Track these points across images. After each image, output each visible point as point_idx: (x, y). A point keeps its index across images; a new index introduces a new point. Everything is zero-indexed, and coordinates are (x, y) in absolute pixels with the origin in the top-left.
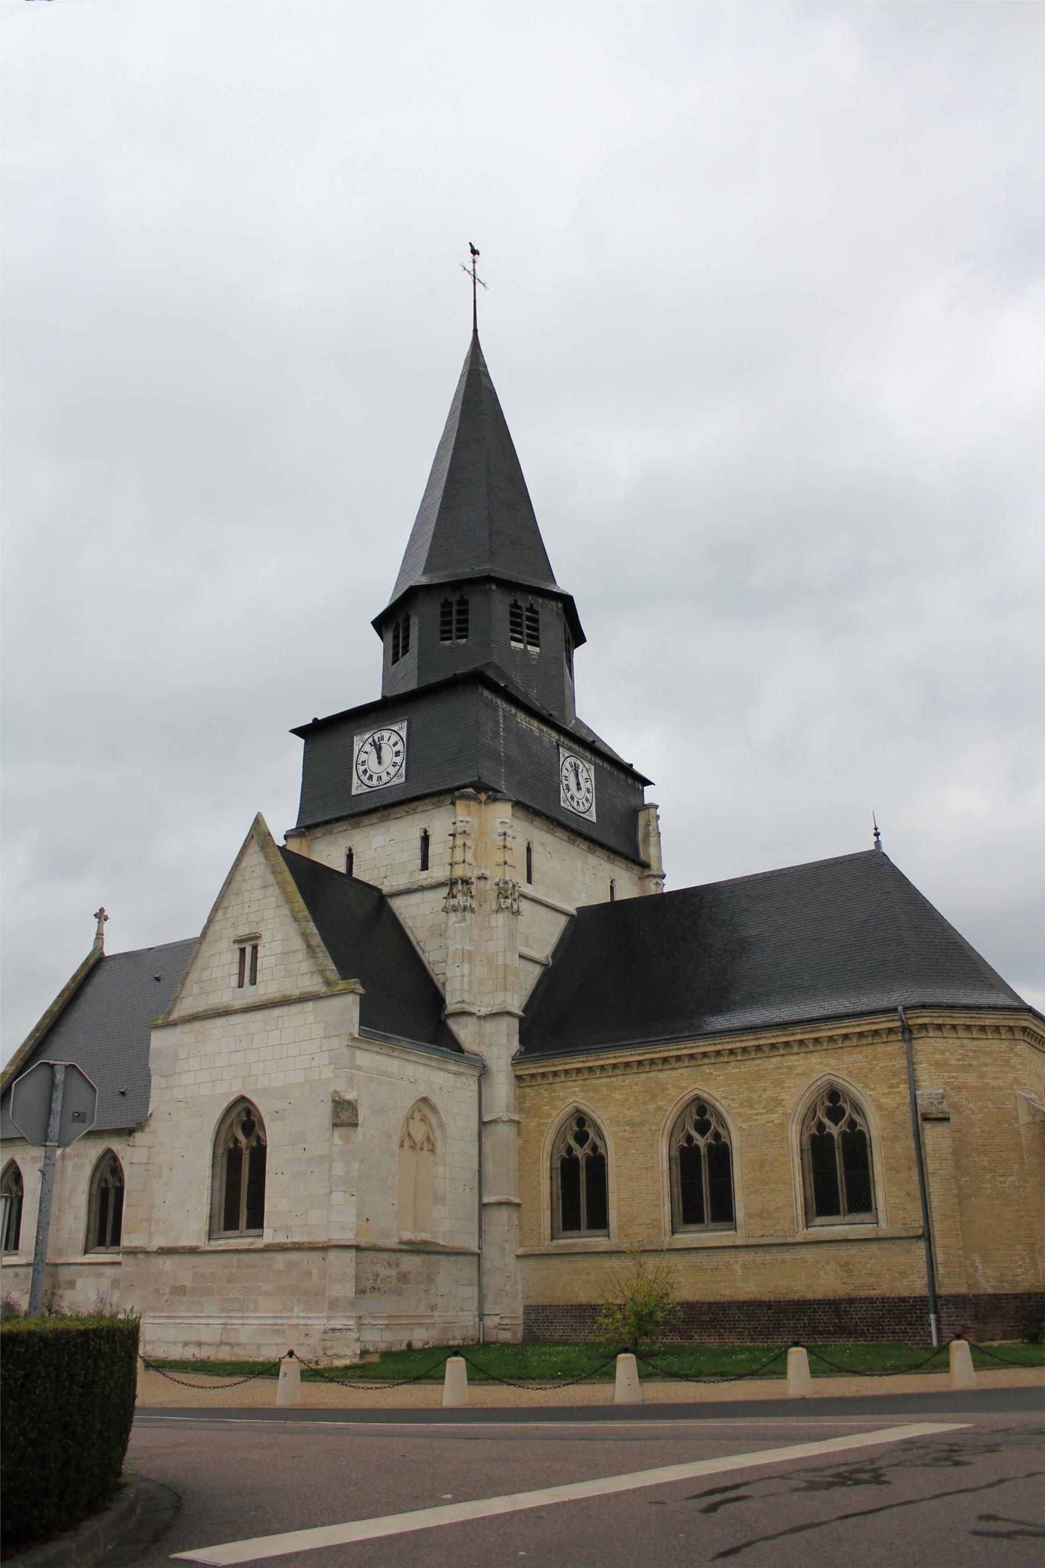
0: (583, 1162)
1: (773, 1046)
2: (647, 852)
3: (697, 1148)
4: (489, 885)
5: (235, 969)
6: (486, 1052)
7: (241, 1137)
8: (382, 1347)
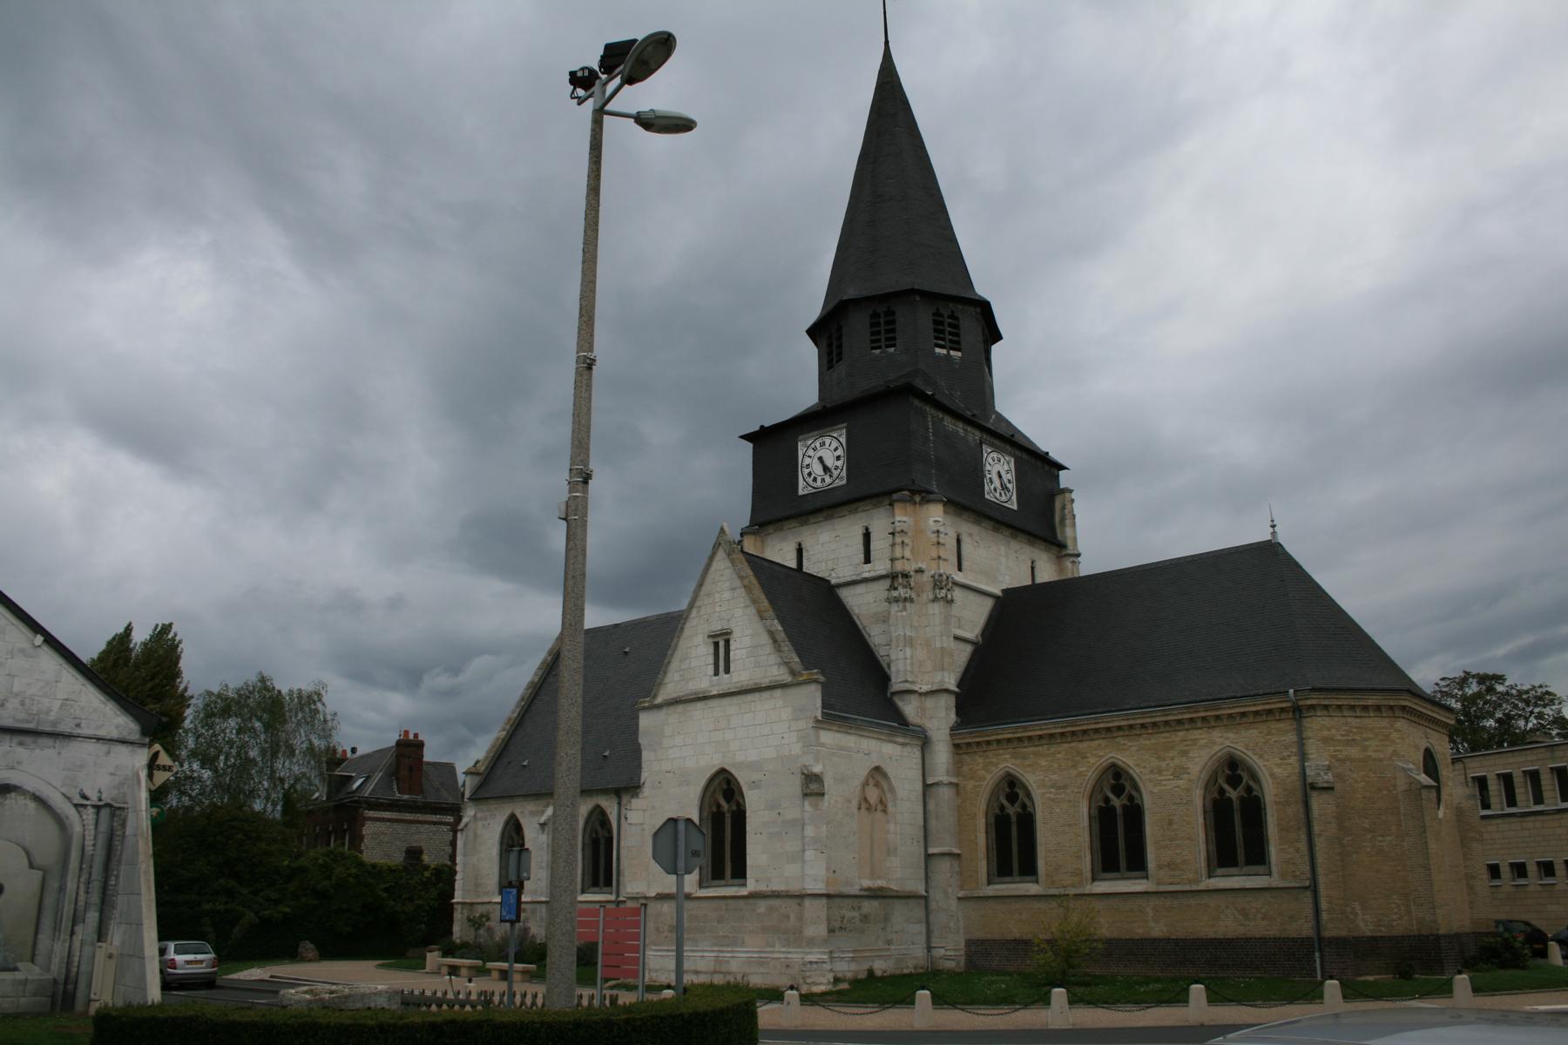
0: (1014, 819)
1: (1179, 722)
2: (1063, 532)
3: (1114, 808)
4: (926, 578)
5: (711, 660)
6: (928, 724)
7: (723, 802)
8: (849, 975)
